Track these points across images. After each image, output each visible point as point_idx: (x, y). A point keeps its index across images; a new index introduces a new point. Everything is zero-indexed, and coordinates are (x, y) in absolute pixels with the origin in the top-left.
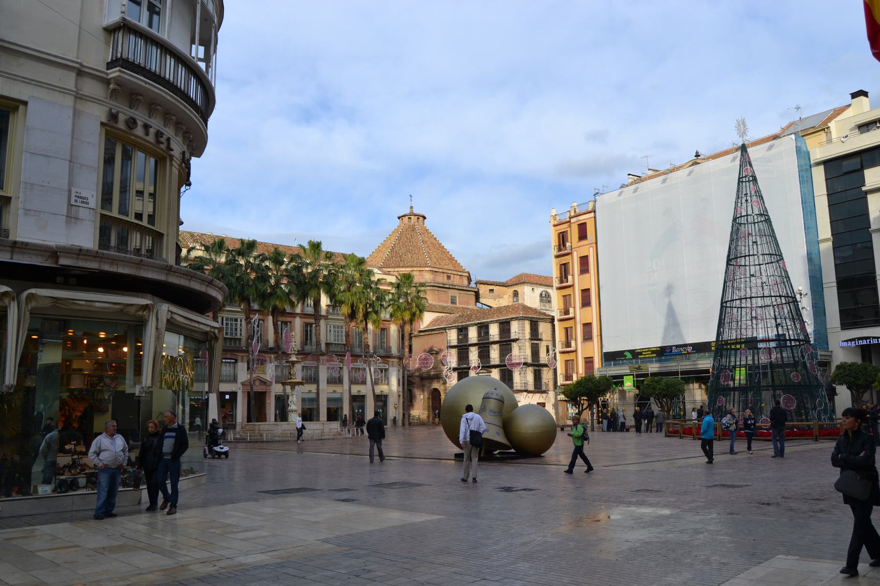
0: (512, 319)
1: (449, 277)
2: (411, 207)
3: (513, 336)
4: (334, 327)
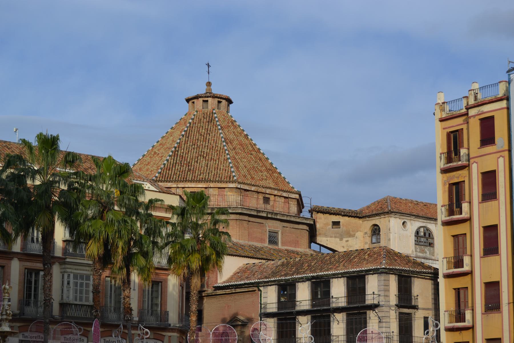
0: (368, 272)
1: (266, 200)
2: (209, 84)
3: (369, 300)
4: (76, 277)
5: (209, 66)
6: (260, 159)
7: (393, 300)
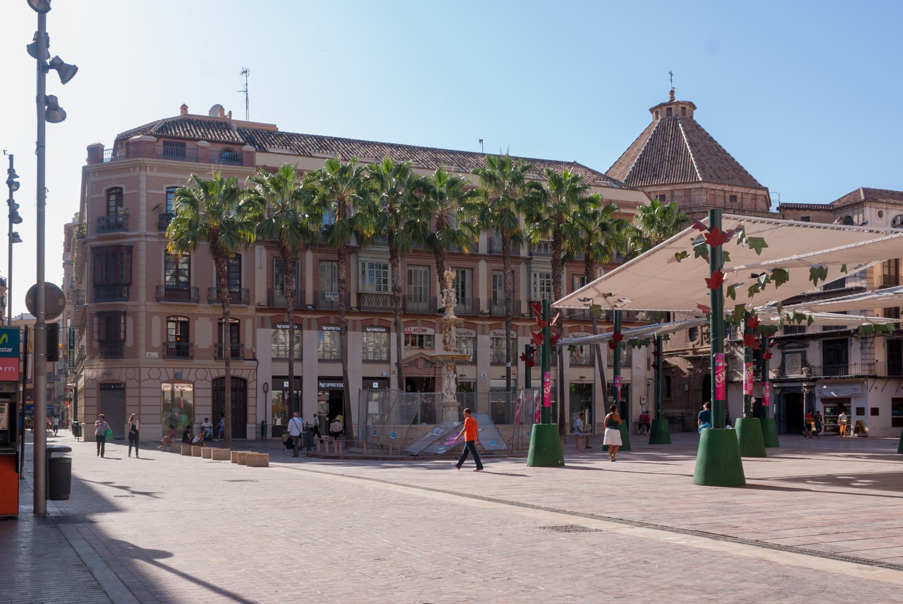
2: (672, 92)
6: (726, 160)
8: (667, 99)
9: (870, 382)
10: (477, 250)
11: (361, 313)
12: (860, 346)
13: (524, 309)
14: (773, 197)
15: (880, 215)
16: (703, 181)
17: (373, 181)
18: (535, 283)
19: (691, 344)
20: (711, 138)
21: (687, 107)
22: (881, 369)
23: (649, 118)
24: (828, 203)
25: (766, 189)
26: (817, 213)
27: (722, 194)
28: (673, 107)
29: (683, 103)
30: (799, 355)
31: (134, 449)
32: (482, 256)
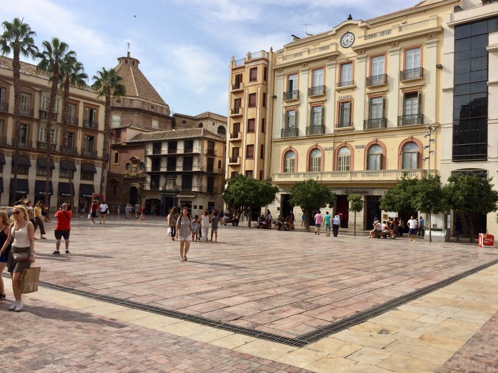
0: (195, 138)
2: (129, 53)
5: (129, 44)
7: (205, 152)
8: (126, 56)
9: (199, 195)
10: (7, 110)
11: (37, 151)
12: (196, 178)
13: (34, 145)
14: (171, 110)
15: (214, 124)
16: (139, 97)
17: (149, 161)
18: (42, 133)
19: (127, 171)
20: (145, 78)
21: (135, 62)
22: (205, 190)
23: (117, 63)
24: (194, 116)
25: (167, 106)
26: (189, 120)
27: (148, 104)
28: (129, 60)
29: (133, 59)
30: (173, 180)
31: (497, 121)
32: (11, 115)
